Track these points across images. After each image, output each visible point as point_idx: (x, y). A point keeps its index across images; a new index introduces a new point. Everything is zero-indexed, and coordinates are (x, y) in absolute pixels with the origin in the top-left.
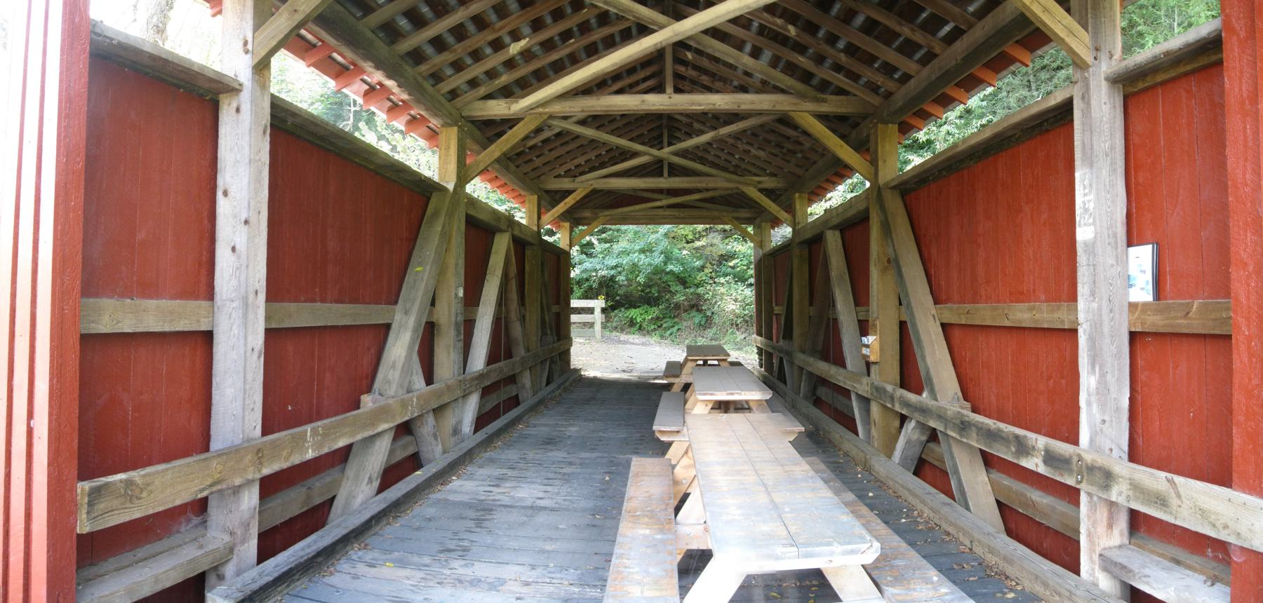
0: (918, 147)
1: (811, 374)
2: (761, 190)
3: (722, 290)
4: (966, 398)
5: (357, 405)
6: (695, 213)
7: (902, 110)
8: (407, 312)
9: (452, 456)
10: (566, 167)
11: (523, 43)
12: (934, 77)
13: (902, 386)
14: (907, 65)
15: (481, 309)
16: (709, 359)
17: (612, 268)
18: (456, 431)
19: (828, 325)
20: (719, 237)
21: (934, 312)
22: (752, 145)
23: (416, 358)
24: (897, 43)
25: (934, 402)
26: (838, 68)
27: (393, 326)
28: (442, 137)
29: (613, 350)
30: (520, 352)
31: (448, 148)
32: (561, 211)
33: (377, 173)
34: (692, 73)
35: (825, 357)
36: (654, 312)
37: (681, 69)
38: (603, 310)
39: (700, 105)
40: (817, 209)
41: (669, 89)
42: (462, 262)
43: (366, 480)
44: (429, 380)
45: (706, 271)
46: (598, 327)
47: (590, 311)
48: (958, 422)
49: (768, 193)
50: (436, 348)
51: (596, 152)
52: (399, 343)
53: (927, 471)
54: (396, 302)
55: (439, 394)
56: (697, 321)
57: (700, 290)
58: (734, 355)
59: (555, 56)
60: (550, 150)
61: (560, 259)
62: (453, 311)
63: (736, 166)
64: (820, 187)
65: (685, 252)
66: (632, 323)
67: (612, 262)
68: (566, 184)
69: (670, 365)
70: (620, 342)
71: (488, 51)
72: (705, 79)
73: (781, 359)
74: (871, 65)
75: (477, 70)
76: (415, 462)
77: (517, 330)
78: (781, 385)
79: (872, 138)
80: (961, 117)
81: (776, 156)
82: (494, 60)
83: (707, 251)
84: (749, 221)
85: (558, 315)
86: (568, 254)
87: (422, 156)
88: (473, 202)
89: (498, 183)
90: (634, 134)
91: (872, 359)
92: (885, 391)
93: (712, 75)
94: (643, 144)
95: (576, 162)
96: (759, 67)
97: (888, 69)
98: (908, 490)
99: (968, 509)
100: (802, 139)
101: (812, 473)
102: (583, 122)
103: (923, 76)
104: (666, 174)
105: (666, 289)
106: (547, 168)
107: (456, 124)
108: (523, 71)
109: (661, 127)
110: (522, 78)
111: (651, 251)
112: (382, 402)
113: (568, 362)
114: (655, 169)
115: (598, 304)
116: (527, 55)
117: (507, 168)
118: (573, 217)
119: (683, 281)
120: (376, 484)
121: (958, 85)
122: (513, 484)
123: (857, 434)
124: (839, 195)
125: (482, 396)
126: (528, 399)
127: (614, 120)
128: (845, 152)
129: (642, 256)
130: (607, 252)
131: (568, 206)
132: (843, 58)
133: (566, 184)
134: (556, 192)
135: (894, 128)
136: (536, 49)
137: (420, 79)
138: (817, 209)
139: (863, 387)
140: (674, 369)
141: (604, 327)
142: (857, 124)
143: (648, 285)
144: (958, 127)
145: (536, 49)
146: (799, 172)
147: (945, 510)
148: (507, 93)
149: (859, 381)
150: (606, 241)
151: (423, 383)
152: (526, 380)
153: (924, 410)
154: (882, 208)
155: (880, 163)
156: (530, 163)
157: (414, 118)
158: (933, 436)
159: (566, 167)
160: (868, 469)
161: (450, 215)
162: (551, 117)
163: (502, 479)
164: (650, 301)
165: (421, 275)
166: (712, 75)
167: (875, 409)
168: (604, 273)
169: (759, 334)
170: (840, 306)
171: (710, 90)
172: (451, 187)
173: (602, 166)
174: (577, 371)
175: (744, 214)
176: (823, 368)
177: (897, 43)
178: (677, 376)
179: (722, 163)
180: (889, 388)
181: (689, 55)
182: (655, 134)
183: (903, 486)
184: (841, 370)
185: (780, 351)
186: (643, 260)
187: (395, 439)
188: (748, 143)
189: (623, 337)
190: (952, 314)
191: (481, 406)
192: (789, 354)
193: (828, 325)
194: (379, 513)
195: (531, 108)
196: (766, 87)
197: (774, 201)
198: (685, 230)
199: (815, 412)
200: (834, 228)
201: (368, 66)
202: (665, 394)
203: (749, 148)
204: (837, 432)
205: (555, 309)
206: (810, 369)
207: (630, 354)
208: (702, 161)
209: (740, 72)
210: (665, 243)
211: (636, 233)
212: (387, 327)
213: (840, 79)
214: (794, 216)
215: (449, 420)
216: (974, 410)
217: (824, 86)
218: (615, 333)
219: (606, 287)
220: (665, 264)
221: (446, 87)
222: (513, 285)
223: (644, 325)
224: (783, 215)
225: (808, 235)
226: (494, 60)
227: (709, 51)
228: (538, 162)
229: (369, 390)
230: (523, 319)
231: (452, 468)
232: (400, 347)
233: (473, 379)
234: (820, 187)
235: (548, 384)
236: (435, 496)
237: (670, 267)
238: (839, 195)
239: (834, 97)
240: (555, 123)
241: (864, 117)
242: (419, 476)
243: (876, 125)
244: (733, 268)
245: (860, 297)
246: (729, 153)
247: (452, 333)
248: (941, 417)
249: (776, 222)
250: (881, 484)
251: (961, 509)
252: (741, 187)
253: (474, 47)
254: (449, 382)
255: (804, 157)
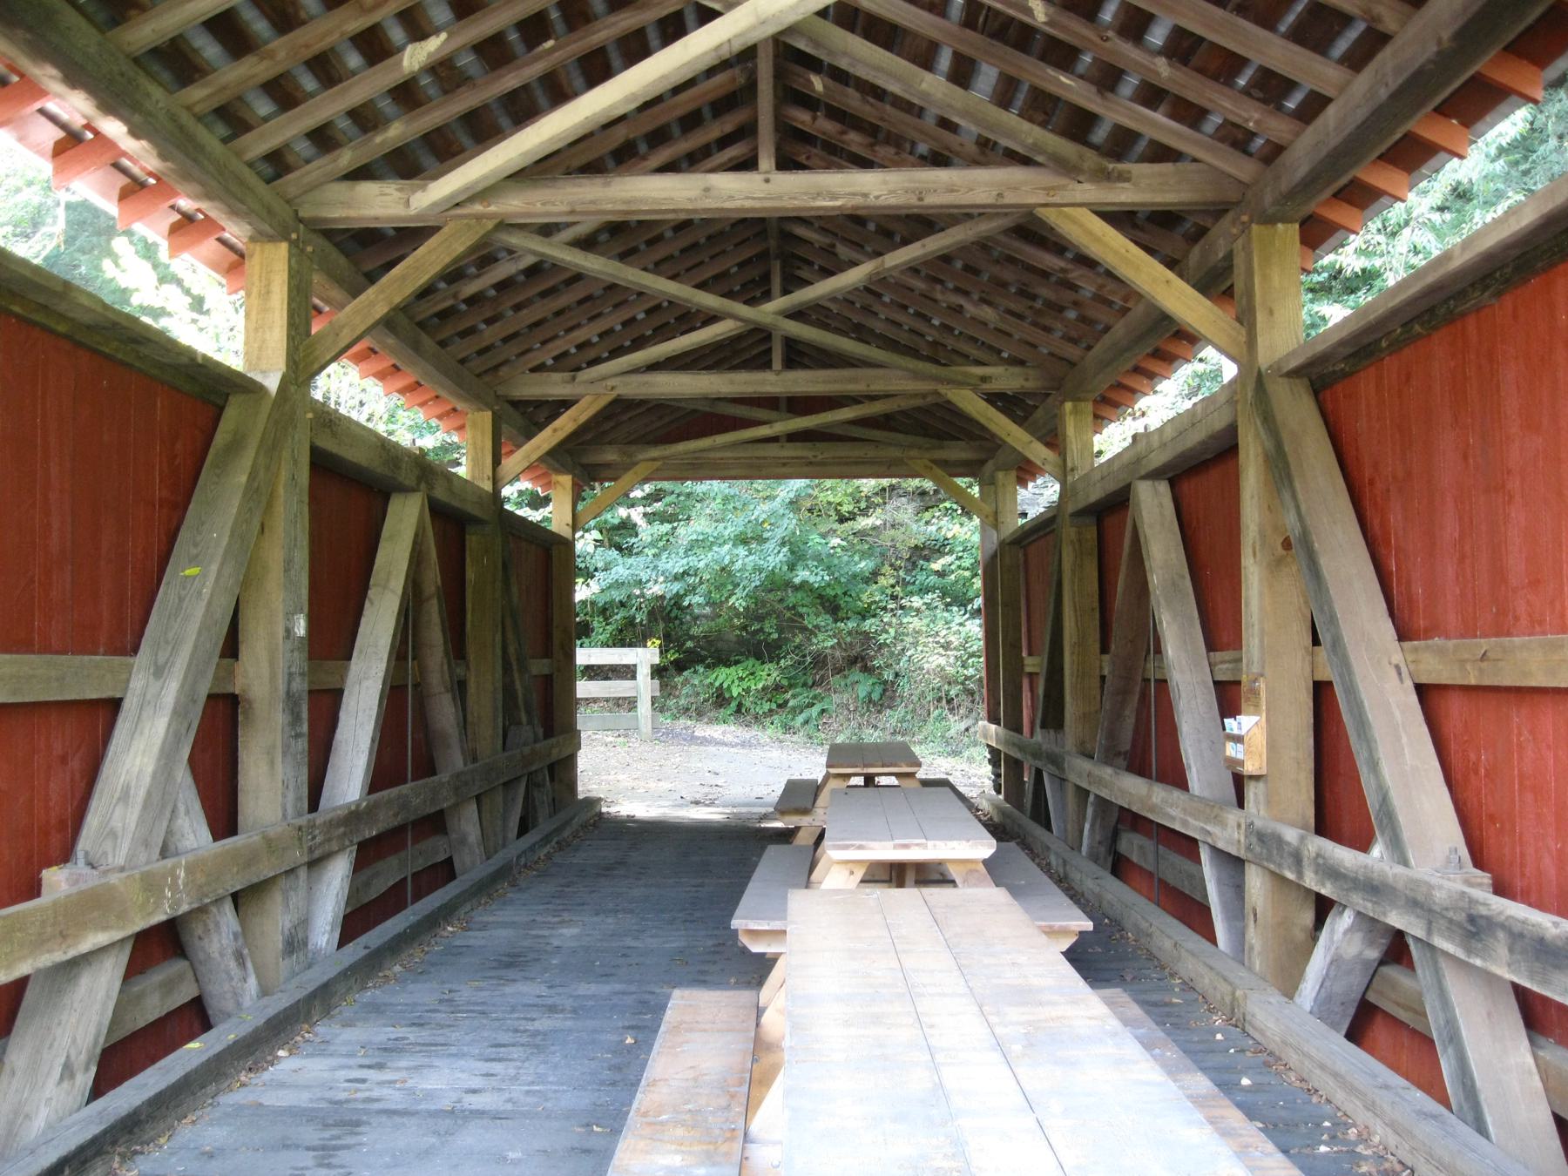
0: (1341, 285)
1: (1103, 804)
2: (994, 399)
3: (915, 623)
4: (1478, 862)
5: (33, 889)
6: (843, 450)
7: (1309, 185)
8: (159, 672)
9: (280, 1002)
10: (557, 347)
11: (433, 46)
12: (1383, 94)
13: (1322, 829)
14: (1313, 71)
15: (356, 665)
16: (872, 771)
17: (677, 578)
18: (295, 943)
19: (1144, 696)
20: (911, 508)
21: (1397, 658)
22: (966, 293)
23: (183, 775)
24: (1291, 18)
25: (1399, 869)
26: (1151, 95)
27: (126, 705)
28: (253, 265)
29: (676, 756)
30: (453, 761)
31: (267, 293)
32: (546, 447)
33: (79, 345)
34: (825, 126)
35: (1138, 766)
36: (769, 674)
37: (801, 118)
38: (658, 672)
39: (834, 197)
40: (1112, 440)
41: (766, 162)
42: (302, 557)
43: (57, 1071)
44: (224, 820)
45: (883, 581)
46: (644, 707)
47: (628, 672)
48: (1461, 917)
49: (1005, 402)
50: (243, 755)
51: (625, 314)
52: (139, 744)
53: (1379, 1032)
54: (135, 650)
55: (251, 859)
56: (862, 691)
57: (870, 625)
58: (934, 765)
59: (510, 81)
60: (518, 308)
61: (550, 559)
62: (281, 665)
63: (935, 344)
64: (1120, 386)
65: (835, 541)
66: (721, 699)
67: (676, 564)
68: (554, 386)
69: (793, 788)
70: (693, 739)
71: (354, 60)
72: (855, 141)
73: (1039, 773)
74: (1229, 82)
75: (328, 107)
76: (196, 1016)
77: (444, 713)
78: (1038, 831)
79: (1239, 261)
80: (1441, 209)
81: (1020, 317)
82: (367, 85)
83: (886, 538)
84: (971, 468)
85: (548, 680)
86: (568, 545)
87: (203, 302)
88: (328, 420)
89: (401, 383)
90: (708, 273)
91: (1250, 768)
92: (1279, 841)
93: (872, 131)
94: (729, 295)
95: (580, 335)
96: (974, 106)
97: (1272, 87)
98: (1336, 1075)
99: (1481, 1129)
100: (1077, 274)
101: (1114, 1023)
102: (587, 243)
103: (1354, 95)
104: (777, 362)
105: (793, 622)
106: (512, 350)
107: (285, 237)
108: (441, 113)
109: (766, 251)
110: (439, 130)
111: (761, 540)
112: (91, 879)
113: (572, 785)
114: (748, 350)
115: (645, 657)
116: (444, 72)
117: (416, 347)
118: (582, 461)
119: (832, 606)
120: (85, 1079)
121: (1443, 111)
122: (418, 1060)
123: (1212, 939)
124: (1165, 403)
125: (359, 866)
126: (472, 865)
127: (658, 239)
128: (1178, 298)
129: (741, 551)
130: (664, 544)
131: (561, 435)
132: (1163, 70)
133: (554, 386)
134: (539, 404)
135: (1289, 233)
136: (467, 60)
137: (186, 119)
138: (1112, 440)
139: (1228, 833)
140: (800, 796)
141: (658, 706)
142: (1201, 232)
143: (755, 614)
144: (1439, 235)
145: (467, 60)
146: (1072, 352)
147: (1425, 1130)
148: (405, 165)
149: (1219, 821)
150: (664, 518)
151: (205, 833)
152: (468, 824)
153: (1374, 888)
154: (1268, 420)
155: (1260, 317)
156: (465, 328)
157: (188, 218)
158: (1397, 949)
159: (557, 347)
160: (1238, 1021)
161: (271, 447)
162: (504, 225)
163: (393, 1049)
164: (763, 651)
165: (194, 589)
166: (872, 131)
167: (1255, 882)
168: (656, 589)
169: (993, 718)
170: (1171, 649)
171: (865, 164)
172: (272, 383)
173: (639, 343)
174: (592, 803)
175: (958, 452)
176: (1133, 790)
177: (1291, 18)
178: (805, 812)
179: (903, 338)
180: (1291, 835)
181: (818, 83)
182: (754, 273)
183: (1322, 1067)
184: (1177, 794)
185: (1036, 755)
186: (743, 559)
187: (134, 970)
188: (957, 290)
189: (703, 730)
190: (1441, 661)
191: (354, 892)
192: (1056, 760)
193: (1144, 696)
194: (82, 1149)
195: (457, 203)
196: (988, 152)
197: (1020, 421)
198: (835, 491)
199: (1115, 892)
200: (1154, 475)
201: (47, 75)
202: (772, 851)
203: (961, 301)
204: (1167, 933)
205: (539, 667)
206: (1104, 794)
207: (713, 766)
208: (860, 333)
209: (929, 121)
210: (789, 523)
211: (726, 499)
212: (115, 705)
213: (1157, 124)
214: (1063, 455)
215: (276, 919)
216: (1500, 889)
217: (1122, 144)
218: (683, 722)
219: (664, 621)
220: (792, 567)
221: (258, 144)
222: (433, 613)
223: (747, 702)
224: (1038, 452)
225: (1095, 495)
226: (367, 85)
227: (861, 72)
228: (490, 334)
229: (65, 855)
230: (460, 689)
231: (279, 1030)
232: (144, 751)
233: (331, 824)
234: (1120, 386)
235: (523, 829)
236: (231, 1099)
237: (802, 575)
238: (1165, 403)
239: (1146, 168)
240: (514, 240)
241: (1219, 211)
242: (196, 1050)
243: (1245, 228)
244: (941, 574)
245: (1219, 626)
246: (918, 314)
247: (280, 718)
248: (1417, 904)
249: (1026, 471)
250: (1269, 1060)
251: (1467, 1132)
252: (943, 389)
253: (318, 47)
254: (272, 832)
255: (1083, 319)
